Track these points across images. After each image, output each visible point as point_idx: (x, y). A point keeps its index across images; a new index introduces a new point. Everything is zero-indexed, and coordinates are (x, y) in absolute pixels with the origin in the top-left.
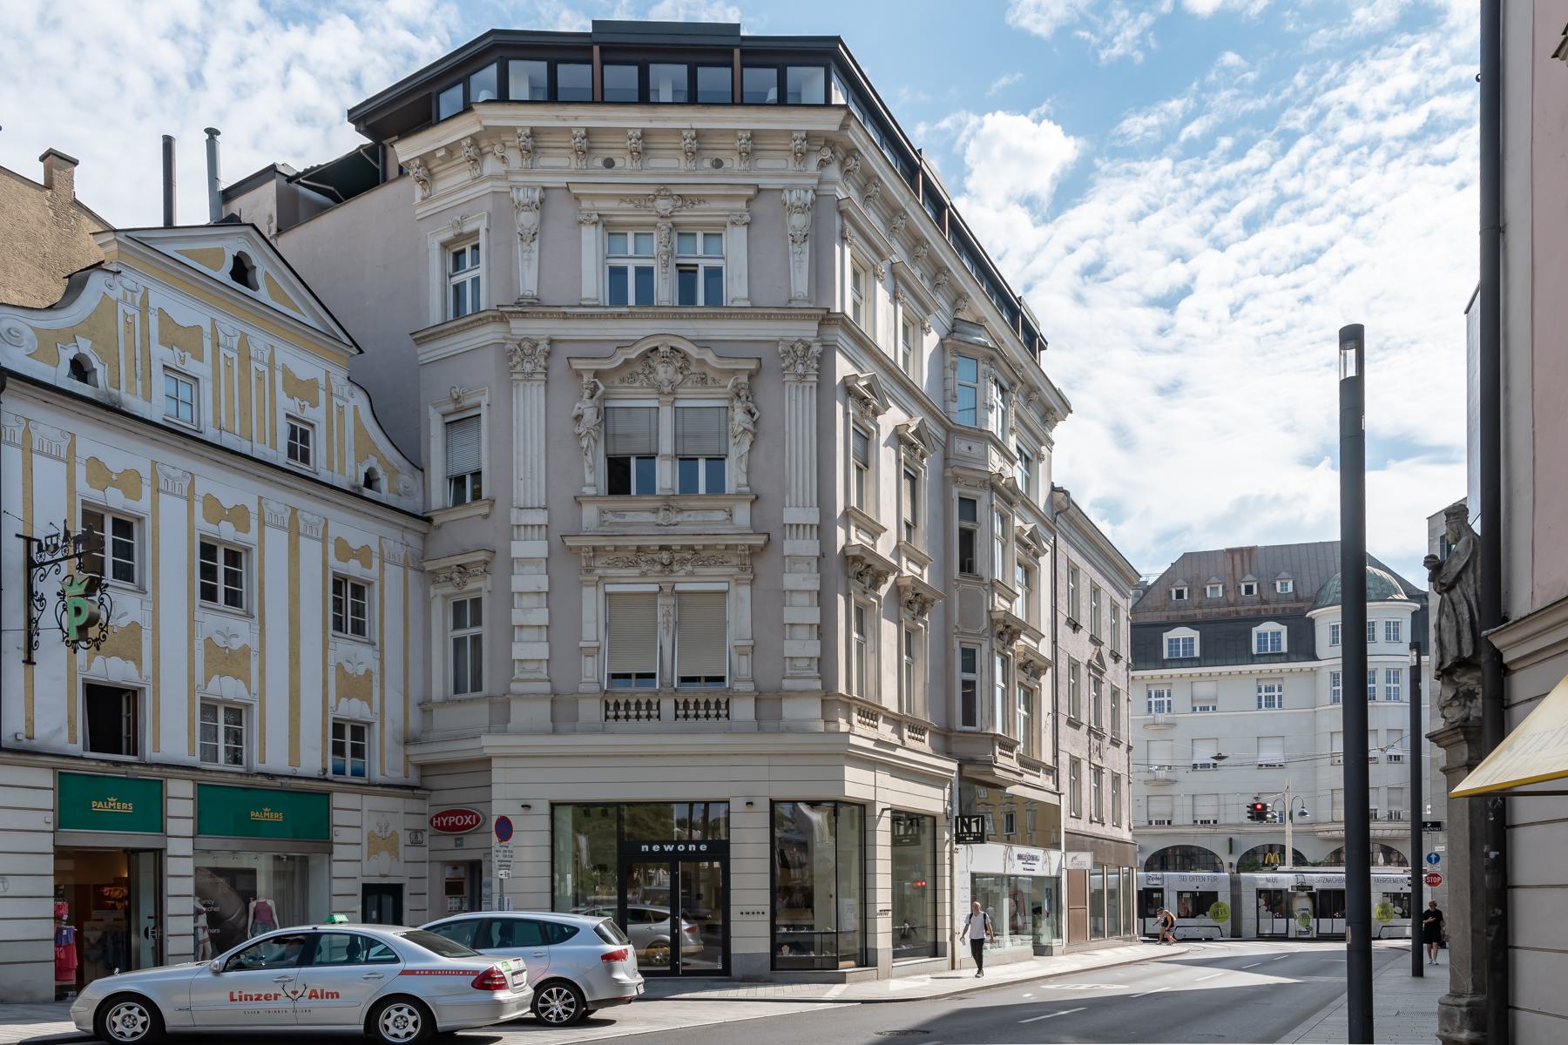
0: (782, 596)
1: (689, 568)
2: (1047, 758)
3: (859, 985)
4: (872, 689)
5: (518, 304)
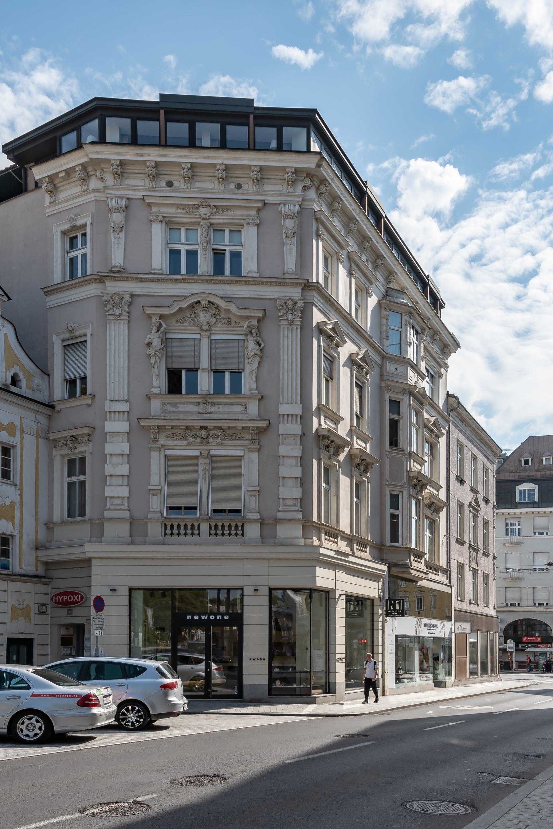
1: (219, 440)
2: (443, 563)
3: (323, 706)
4: (334, 518)
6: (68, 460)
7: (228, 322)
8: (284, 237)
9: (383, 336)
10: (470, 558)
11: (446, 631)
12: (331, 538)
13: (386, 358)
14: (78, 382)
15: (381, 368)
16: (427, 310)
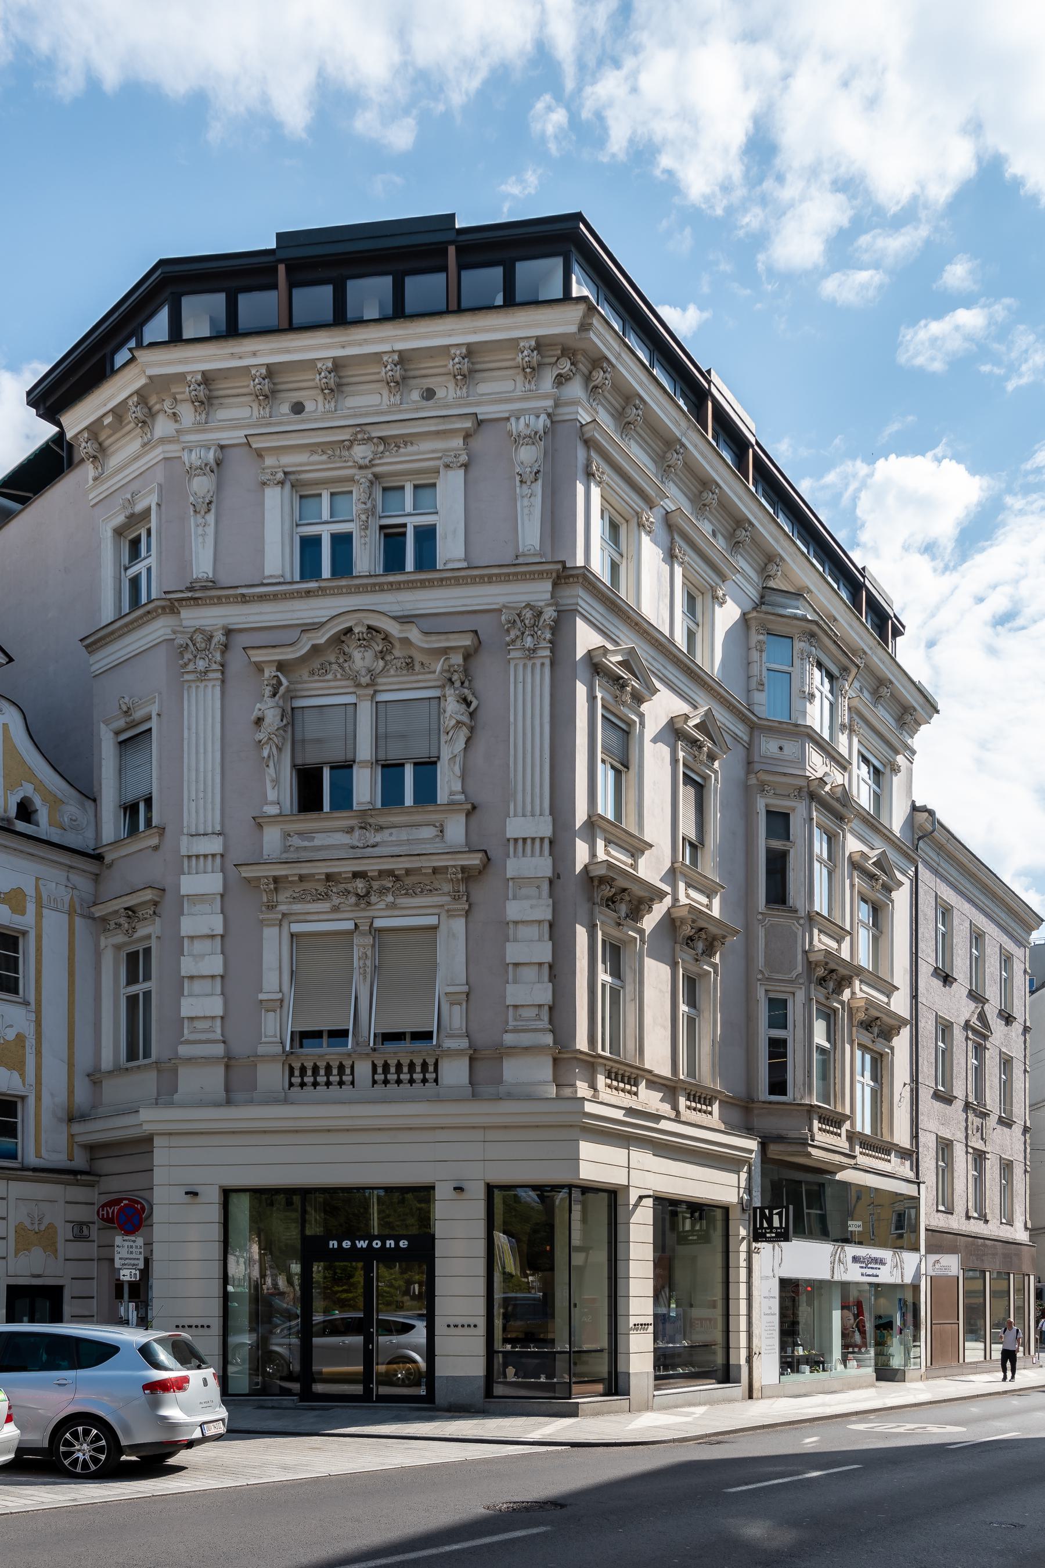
0: (505, 928)
1: (390, 898)
2: (902, 1137)
3: (597, 1422)
4: (631, 1045)
5: (190, 589)
6: (128, 954)
7: (408, 664)
8: (518, 483)
9: (754, 684)
10: (966, 1128)
11: (905, 1272)
12: (621, 1085)
13: (758, 728)
14: (142, 806)
15: (749, 749)
16: (857, 634)
